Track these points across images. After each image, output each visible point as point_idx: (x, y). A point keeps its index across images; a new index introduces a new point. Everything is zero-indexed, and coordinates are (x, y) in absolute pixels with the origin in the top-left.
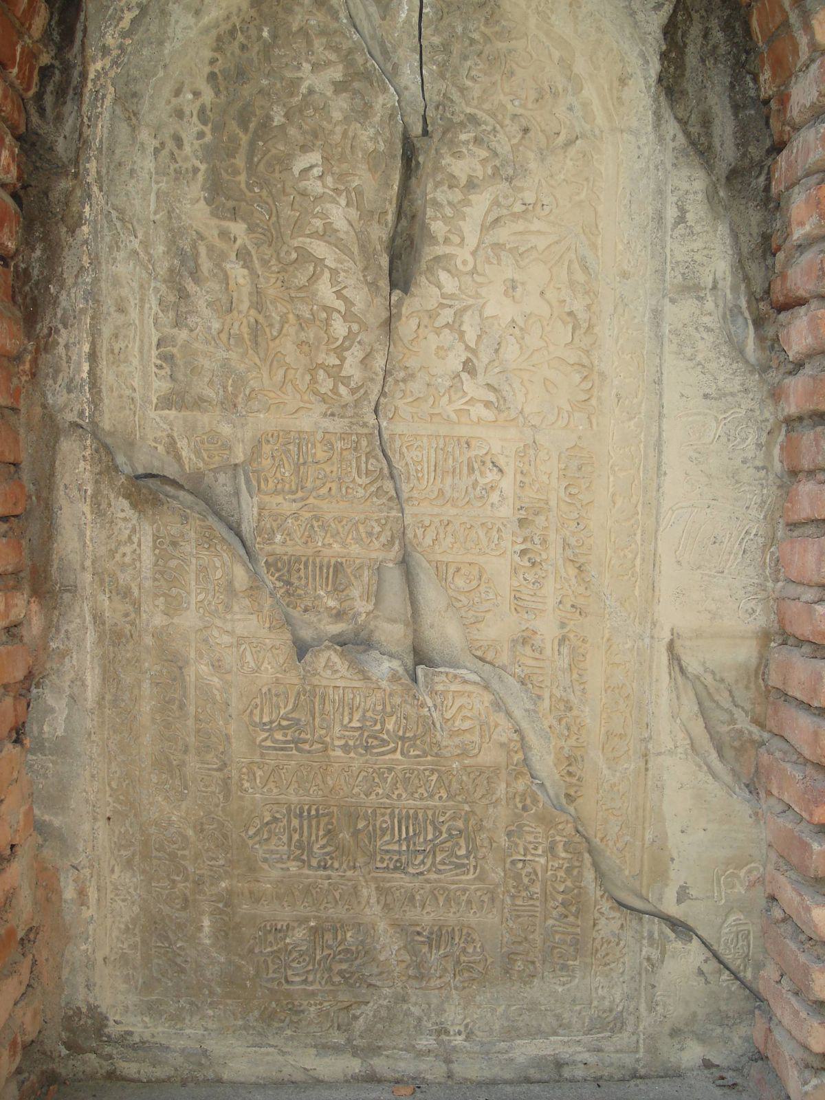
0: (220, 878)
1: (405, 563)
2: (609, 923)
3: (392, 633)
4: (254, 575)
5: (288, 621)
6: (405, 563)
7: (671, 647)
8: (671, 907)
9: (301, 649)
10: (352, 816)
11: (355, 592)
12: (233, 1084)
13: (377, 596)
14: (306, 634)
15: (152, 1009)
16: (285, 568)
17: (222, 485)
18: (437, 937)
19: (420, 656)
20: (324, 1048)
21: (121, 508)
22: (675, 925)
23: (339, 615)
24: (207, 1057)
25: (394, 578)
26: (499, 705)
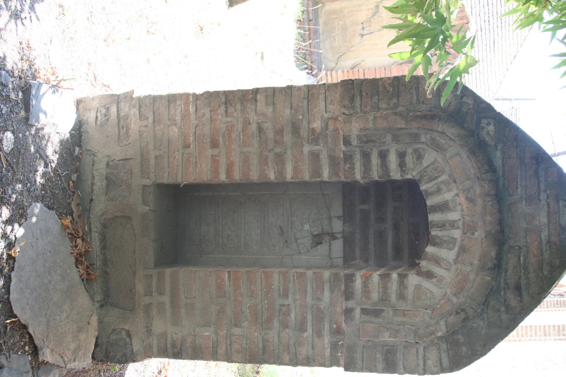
0: (24, 165)
1: (371, 33)
2: (337, 57)
3: (365, 32)
4: (370, 18)
5: (365, 22)
6: (371, 33)
7: (364, 60)
8: (338, 63)
9: (362, 23)
10: (346, 30)
11: (368, 28)
12: (447, 328)
13: (368, 30)
14: (364, 24)
15: (325, 12)
16: (370, 21)
17: (378, 14)
18: (335, 39)
19: (362, 35)
20: (322, 29)
21: (375, 4)
22: (337, 64)
23: (366, 27)
24: (313, 298)
25: (370, 32)
26: (358, 43)
